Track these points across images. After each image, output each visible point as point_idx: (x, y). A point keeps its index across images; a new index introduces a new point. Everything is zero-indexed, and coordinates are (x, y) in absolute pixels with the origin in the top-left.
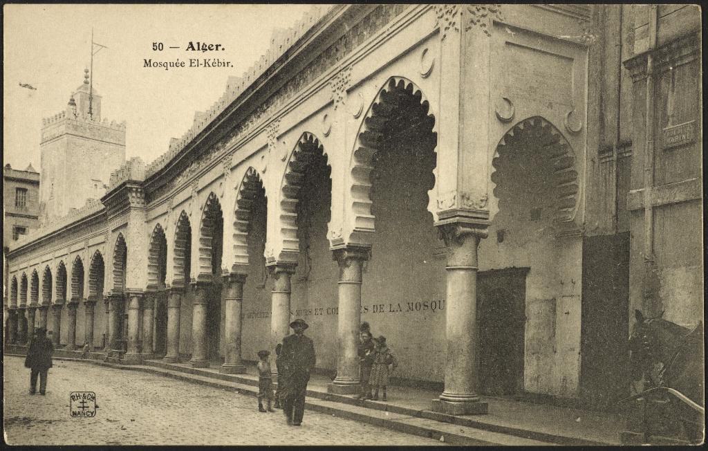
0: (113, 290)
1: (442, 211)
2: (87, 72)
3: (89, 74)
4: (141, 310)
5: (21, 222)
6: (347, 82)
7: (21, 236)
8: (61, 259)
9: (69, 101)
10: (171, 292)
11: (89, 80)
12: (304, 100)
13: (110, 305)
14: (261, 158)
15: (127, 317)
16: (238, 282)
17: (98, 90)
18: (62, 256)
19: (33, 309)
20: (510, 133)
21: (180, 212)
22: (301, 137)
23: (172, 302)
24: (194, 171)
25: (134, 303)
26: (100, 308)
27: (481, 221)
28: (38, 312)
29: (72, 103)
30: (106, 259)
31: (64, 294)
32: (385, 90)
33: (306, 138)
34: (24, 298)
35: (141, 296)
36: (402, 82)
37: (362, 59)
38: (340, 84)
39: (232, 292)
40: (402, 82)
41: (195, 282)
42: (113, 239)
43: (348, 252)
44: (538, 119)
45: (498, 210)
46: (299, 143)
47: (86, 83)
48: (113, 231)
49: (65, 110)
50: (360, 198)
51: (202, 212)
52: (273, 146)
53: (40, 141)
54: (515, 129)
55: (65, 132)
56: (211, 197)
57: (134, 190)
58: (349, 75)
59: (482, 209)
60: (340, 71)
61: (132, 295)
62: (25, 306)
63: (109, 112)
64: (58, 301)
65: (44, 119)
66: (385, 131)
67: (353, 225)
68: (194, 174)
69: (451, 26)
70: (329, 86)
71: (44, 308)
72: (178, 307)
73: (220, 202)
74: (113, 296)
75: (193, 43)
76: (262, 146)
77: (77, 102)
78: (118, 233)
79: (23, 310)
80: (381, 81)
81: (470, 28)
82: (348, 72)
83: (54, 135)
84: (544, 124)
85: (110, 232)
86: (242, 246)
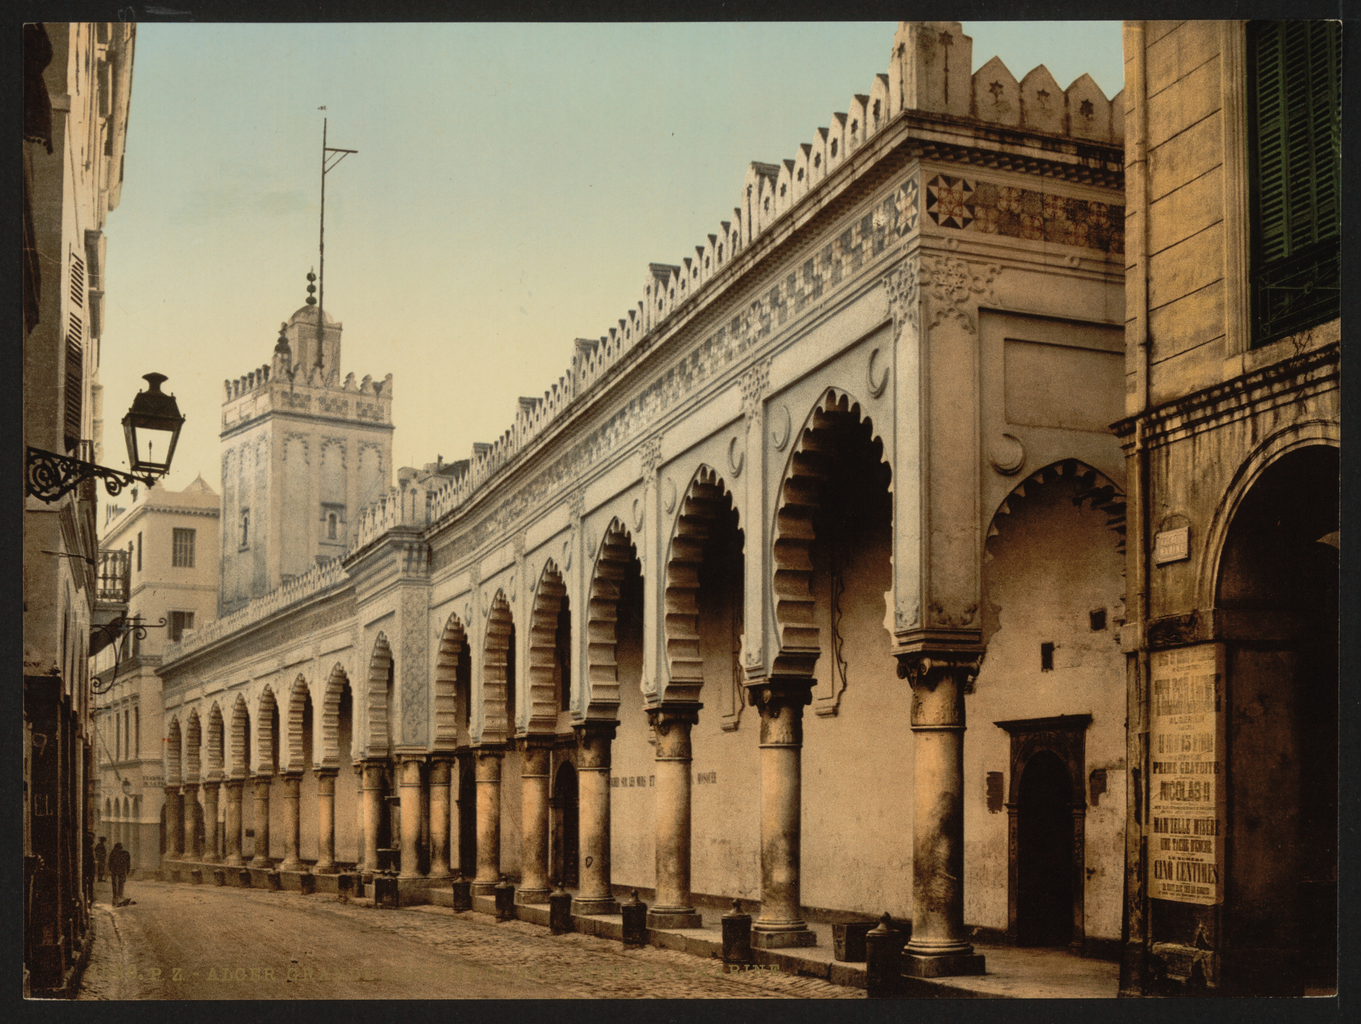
0: (372, 749)
2: (311, 277)
3: (316, 283)
4: (425, 787)
6: (764, 386)
10: (480, 753)
11: (316, 295)
12: (699, 403)
13: (365, 775)
15: (397, 802)
16: (447, 762)
17: (333, 312)
19: (213, 787)
20: (1017, 492)
21: (495, 591)
23: (483, 771)
24: (518, 514)
25: (411, 775)
26: (345, 783)
27: (968, 648)
28: (223, 791)
29: (282, 346)
30: (354, 684)
31: (275, 755)
34: (196, 763)
35: (424, 760)
37: (728, 388)
38: (753, 389)
39: (588, 756)
41: (524, 735)
43: (664, 713)
44: (1070, 464)
47: (311, 301)
48: (368, 626)
49: (269, 363)
50: (682, 630)
51: (534, 593)
53: (220, 430)
54: (1028, 483)
55: (269, 409)
56: (612, 528)
57: (407, 545)
58: (767, 373)
59: (966, 627)
60: (753, 363)
62: (198, 777)
63: (357, 359)
64: (262, 768)
65: (227, 382)
67: (486, 724)
68: (520, 519)
69: (907, 320)
71: (237, 786)
72: (497, 779)
73: (634, 540)
74: (370, 760)
77: (293, 345)
79: (193, 788)
81: (936, 324)
82: (764, 369)
83: (248, 416)
84: (1081, 472)
85: (361, 629)
86: (546, 687)
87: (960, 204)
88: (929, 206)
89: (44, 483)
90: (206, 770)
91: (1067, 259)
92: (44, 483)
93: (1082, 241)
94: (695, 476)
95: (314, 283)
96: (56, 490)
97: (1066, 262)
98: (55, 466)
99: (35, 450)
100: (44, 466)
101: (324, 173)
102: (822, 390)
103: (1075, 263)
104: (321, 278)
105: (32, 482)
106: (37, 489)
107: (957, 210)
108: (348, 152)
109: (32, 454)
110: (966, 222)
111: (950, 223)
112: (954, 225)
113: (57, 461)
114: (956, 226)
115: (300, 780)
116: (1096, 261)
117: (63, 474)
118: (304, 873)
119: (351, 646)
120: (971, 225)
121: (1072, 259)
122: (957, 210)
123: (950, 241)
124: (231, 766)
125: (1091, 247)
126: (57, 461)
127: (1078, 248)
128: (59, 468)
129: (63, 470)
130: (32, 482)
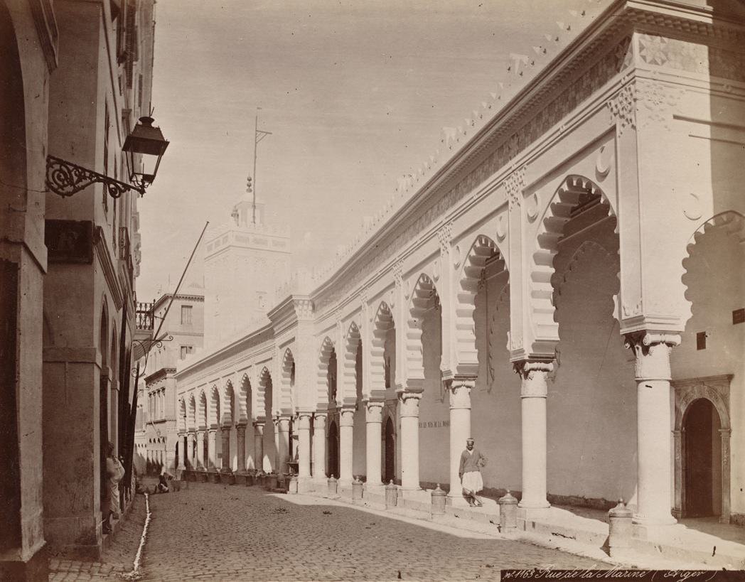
1: (629, 317)
2: (250, 180)
5: (186, 341)
7: (188, 356)
8: (244, 371)
9: (231, 212)
14: (498, 219)
18: (228, 375)
22: (476, 241)
32: (562, 189)
33: (481, 242)
36: (580, 183)
40: (580, 183)
42: (280, 357)
45: (692, 315)
46: (560, 190)
52: (516, 203)
61: (302, 414)
66: (567, 229)
70: (502, 188)
75: (285, 495)
76: (433, 251)
78: (285, 348)
80: (472, 237)
87: (659, 50)
88: (640, 51)
89: (61, 183)
90: (200, 422)
91: (724, 87)
92: (61, 183)
93: (732, 76)
94: (475, 243)
95: (251, 182)
96: (69, 189)
97: (724, 88)
98: (70, 172)
99: (54, 158)
100: (61, 171)
101: (256, 143)
102: (555, 190)
103: (729, 90)
104: (254, 185)
105: (51, 180)
106: (55, 186)
107: (658, 54)
108: (267, 133)
109: (52, 160)
110: (663, 62)
111: (654, 62)
112: (656, 63)
113: (71, 168)
114: (657, 64)
115: (245, 428)
116: (740, 88)
117: (75, 178)
118: (248, 475)
119: (271, 358)
120: (666, 63)
121: (728, 86)
122: (658, 54)
123: (655, 73)
124: (212, 420)
125: (738, 80)
126: (71, 168)
127: (731, 81)
128: (73, 173)
129: (76, 175)
130: (51, 180)
